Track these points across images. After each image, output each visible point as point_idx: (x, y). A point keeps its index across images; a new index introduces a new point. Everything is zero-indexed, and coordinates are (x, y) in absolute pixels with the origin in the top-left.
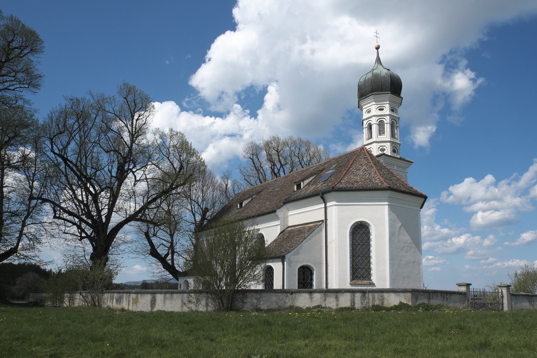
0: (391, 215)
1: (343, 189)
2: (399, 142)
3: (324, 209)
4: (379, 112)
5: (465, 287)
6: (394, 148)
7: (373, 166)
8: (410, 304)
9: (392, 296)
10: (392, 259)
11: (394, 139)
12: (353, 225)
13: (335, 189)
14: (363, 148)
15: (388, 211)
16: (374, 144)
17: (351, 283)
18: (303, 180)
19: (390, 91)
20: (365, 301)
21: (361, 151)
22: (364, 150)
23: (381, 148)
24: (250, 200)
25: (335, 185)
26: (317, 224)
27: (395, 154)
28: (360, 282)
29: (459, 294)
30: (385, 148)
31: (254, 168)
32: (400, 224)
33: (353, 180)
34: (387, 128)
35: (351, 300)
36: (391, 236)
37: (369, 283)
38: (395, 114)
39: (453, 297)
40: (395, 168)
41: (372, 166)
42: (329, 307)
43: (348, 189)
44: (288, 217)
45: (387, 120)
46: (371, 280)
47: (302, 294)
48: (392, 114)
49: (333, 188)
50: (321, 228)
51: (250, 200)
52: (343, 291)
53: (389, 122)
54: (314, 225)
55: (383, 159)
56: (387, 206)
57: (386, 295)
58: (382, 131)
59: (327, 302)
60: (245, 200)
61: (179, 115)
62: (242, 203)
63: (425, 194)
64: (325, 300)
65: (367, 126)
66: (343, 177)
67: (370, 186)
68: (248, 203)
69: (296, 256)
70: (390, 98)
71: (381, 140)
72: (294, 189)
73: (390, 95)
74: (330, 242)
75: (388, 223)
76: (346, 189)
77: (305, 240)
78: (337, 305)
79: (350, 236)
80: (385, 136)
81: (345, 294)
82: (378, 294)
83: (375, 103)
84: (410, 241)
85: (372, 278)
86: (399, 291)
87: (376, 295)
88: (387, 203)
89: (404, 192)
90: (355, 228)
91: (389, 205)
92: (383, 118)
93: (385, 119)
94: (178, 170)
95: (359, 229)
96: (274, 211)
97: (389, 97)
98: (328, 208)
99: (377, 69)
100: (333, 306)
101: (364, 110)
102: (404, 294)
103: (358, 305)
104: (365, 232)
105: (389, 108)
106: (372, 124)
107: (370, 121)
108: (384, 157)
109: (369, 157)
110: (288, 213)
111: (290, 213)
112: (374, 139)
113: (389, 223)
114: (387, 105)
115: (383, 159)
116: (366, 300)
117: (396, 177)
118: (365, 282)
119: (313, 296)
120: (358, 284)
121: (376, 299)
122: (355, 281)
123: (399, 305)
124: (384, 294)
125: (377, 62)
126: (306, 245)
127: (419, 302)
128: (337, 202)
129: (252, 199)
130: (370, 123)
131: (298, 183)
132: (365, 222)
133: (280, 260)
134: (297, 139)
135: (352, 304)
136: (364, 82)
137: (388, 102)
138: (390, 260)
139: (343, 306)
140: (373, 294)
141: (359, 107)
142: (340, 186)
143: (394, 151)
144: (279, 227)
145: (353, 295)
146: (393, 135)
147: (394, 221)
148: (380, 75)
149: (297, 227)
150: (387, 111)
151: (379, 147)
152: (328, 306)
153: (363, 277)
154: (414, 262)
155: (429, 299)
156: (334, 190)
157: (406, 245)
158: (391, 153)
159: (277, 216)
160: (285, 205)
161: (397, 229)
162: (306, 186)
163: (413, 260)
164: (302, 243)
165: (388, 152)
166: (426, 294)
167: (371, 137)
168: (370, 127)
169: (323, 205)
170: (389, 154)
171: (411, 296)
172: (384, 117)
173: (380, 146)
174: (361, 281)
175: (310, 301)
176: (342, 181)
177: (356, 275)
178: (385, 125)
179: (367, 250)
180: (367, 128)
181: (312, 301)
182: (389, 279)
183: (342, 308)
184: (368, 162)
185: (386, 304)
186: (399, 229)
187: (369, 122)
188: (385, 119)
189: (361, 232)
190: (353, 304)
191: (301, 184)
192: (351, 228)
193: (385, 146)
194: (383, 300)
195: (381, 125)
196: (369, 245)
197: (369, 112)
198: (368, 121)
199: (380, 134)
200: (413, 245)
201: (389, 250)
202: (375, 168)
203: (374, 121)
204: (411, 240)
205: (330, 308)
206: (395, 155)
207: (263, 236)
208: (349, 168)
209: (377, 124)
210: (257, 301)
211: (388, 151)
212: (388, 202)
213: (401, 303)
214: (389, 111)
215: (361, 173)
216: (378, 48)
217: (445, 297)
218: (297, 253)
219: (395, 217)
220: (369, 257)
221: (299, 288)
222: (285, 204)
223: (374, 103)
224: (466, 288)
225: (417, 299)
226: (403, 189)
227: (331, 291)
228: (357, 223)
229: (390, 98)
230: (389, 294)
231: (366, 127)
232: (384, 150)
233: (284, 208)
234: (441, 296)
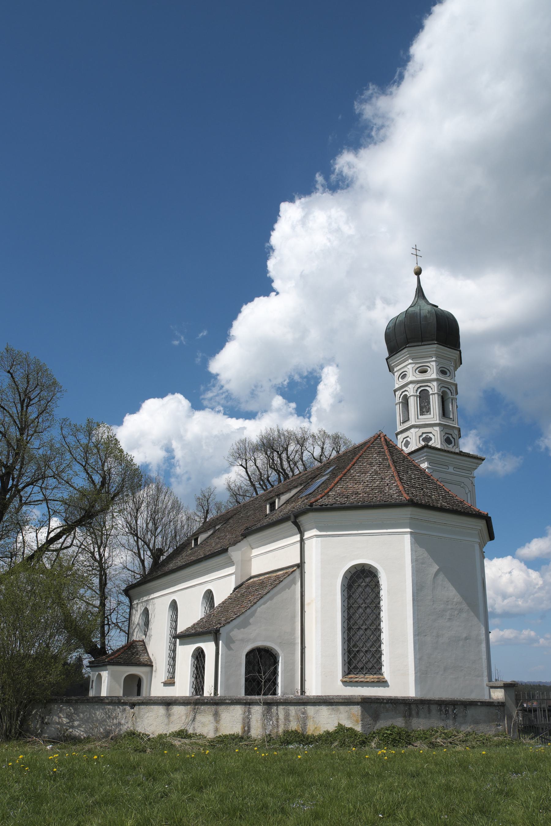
0: (416, 552)
1: (329, 506)
2: (456, 426)
3: (298, 545)
4: (418, 376)
5: (503, 690)
6: (447, 435)
7: (391, 465)
8: (358, 728)
9: (324, 710)
10: (418, 633)
11: (448, 421)
12: (349, 571)
13: (314, 507)
14: (379, 436)
15: (411, 544)
16: (413, 430)
17: (345, 679)
18: (278, 495)
19: (436, 341)
20: (271, 723)
21: (375, 440)
22: (381, 438)
23: (424, 436)
24: (210, 532)
25: (316, 501)
26: (287, 571)
27: (451, 446)
28: (361, 678)
29: (488, 706)
30: (431, 435)
31: (249, 482)
32: (436, 567)
33: (350, 491)
34: (435, 402)
35: (243, 719)
36: (418, 590)
37: (376, 680)
38: (448, 378)
39: (471, 712)
40: (451, 470)
41: (389, 465)
42: (200, 735)
43: (336, 506)
44: (250, 560)
45: (433, 389)
46: (382, 675)
47: (152, 707)
48: (442, 378)
49: (311, 505)
50: (295, 578)
51: (210, 532)
52: (227, 701)
53: (436, 392)
54: (284, 573)
55: (425, 454)
56: (408, 537)
57: (311, 710)
58: (425, 406)
59: (197, 724)
60: (202, 532)
61: (189, 417)
62: (197, 539)
63: (486, 513)
64: (194, 719)
65: (400, 401)
66: (334, 486)
67: (378, 498)
68: (208, 538)
69: (242, 630)
70: (436, 351)
71: (424, 423)
72: (266, 512)
73: (436, 346)
74: (309, 604)
75: (411, 567)
76: (334, 506)
77: (262, 601)
78: (216, 730)
79: (343, 591)
80: (432, 416)
81: (232, 707)
82: (296, 707)
83: (412, 362)
84: (458, 598)
85: (384, 669)
86: (337, 701)
87: (293, 710)
88: (409, 530)
89: (441, 510)
90: (352, 577)
91: (411, 533)
92: (427, 386)
93: (429, 387)
94: (98, 487)
95: (360, 578)
96: (224, 551)
97: (435, 349)
98: (307, 542)
99: (416, 305)
100: (208, 733)
101: (396, 374)
102: (347, 708)
103: (256, 732)
104: (371, 584)
105: (437, 369)
106: (408, 396)
107: (405, 391)
108: (426, 452)
109: (386, 451)
110: (251, 553)
111: (255, 552)
112: (412, 422)
113: (412, 567)
114: (432, 363)
115: (425, 454)
116: (271, 720)
117: (436, 484)
118: (370, 678)
119: (173, 711)
120: (357, 682)
121: (291, 718)
122: (352, 676)
123: (336, 732)
124: (309, 707)
125: (417, 295)
126: (261, 609)
127: (382, 724)
128: (320, 530)
129: (214, 532)
130: (406, 395)
131: (271, 501)
132: (370, 566)
133: (211, 637)
134: (318, 432)
135: (244, 727)
136: (394, 328)
137: (434, 359)
138: (415, 635)
139: (228, 733)
140: (287, 707)
141: (390, 371)
142: (325, 501)
143: (448, 441)
144: (233, 577)
145: (247, 709)
146: (444, 413)
147: (423, 563)
148: (418, 315)
149: (261, 578)
150: (433, 374)
151: (421, 434)
152: (198, 731)
153: (366, 668)
154: (466, 639)
155: (408, 716)
156: (312, 508)
157: (450, 607)
158: (441, 444)
159: (230, 558)
160: (245, 539)
161: (430, 577)
162: (283, 505)
163: (464, 635)
164: (255, 606)
165: (436, 442)
166: (402, 708)
167: (406, 419)
168: (405, 401)
169: (297, 538)
170: (439, 446)
171: (362, 712)
172: (429, 384)
173: (423, 433)
174: (362, 676)
175: (166, 721)
176: (330, 493)
177: (354, 665)
178: (431, 396)
179: (375, 616)
180: (401, 405)
181: (168, 724)
182: (414, 672)
183: (226, 736)
184: (383, 459)
185: (311, 729)
186: (434, 578)
187: (403, 394)
188: (429, 387)
189: (363, 584)
190: (246, 728)
191: (275, 502)
192: (345, 577)
193: (431, 433)
194: (304, 720)
195: (424, 397)
196: (377, 608)
197: (404, 376)
198: (402, 392)
199: (422, 413)
200: (465, 606)
201: (413, 616)
202: (393, 468)
203: (411, 390)
204: (459, 596)
205: (202, 736)
206: (450, 448)
207: (213, 595)
208: (349, 470)
209: (417, 396)
210: (68, 721)
211: (436, 441)
212: (410, 528)
213: (340, 725)
214: (437, 373)
215: (368, 479)
216: (418, 272)
217: (450, 712)
218: (245, 624)
219: (426, 554)
220: (378, 630)
221: (247, 693)
222: (245, 537)
223: (410, 361)
224: (505, 690)
225: (376, 717)
226: (441, 503)
227: (206, 701)
228: (355, 567)
229: (436, 351)
230: (317, 708)
231: (400, 402)
232: (430, 439)
233: (243, 545)
234: (441, 710)
